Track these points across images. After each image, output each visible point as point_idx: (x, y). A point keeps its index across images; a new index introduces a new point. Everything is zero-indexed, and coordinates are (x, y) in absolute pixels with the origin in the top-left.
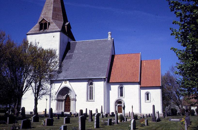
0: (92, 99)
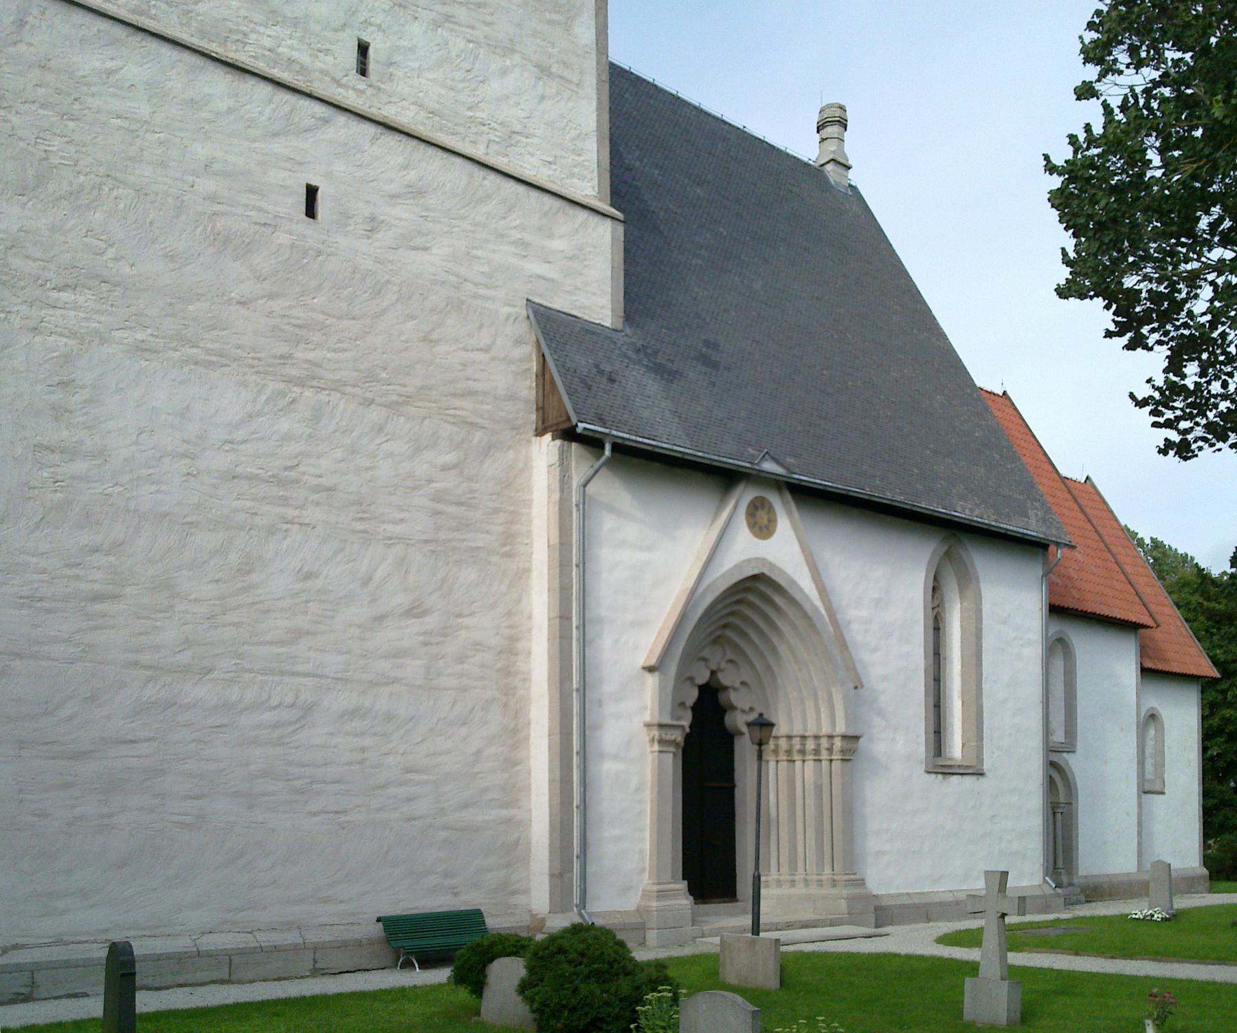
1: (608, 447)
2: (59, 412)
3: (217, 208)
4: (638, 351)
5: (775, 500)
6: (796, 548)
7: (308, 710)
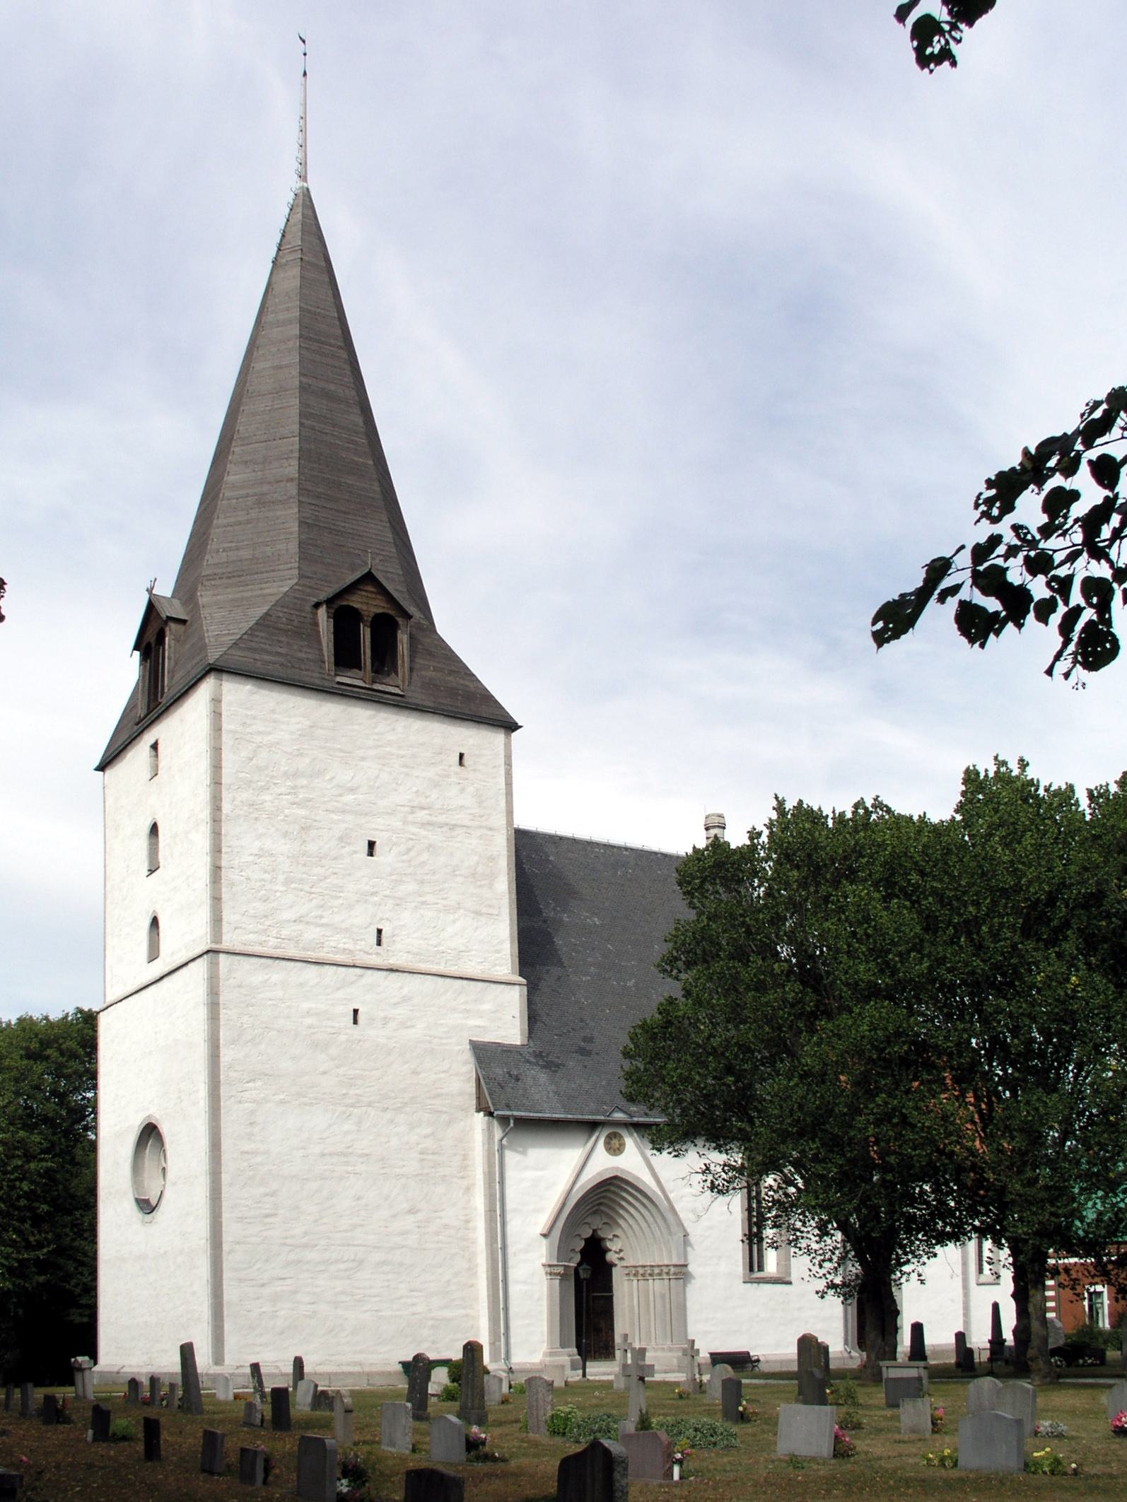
0: (761, 1268)
1: (512, 1121)
2: (250, 1136)
3: (312, 1031)
4: (536, 1056)
5: (624, 1132)
6: (639, 1159)
7: (361, 1262)
